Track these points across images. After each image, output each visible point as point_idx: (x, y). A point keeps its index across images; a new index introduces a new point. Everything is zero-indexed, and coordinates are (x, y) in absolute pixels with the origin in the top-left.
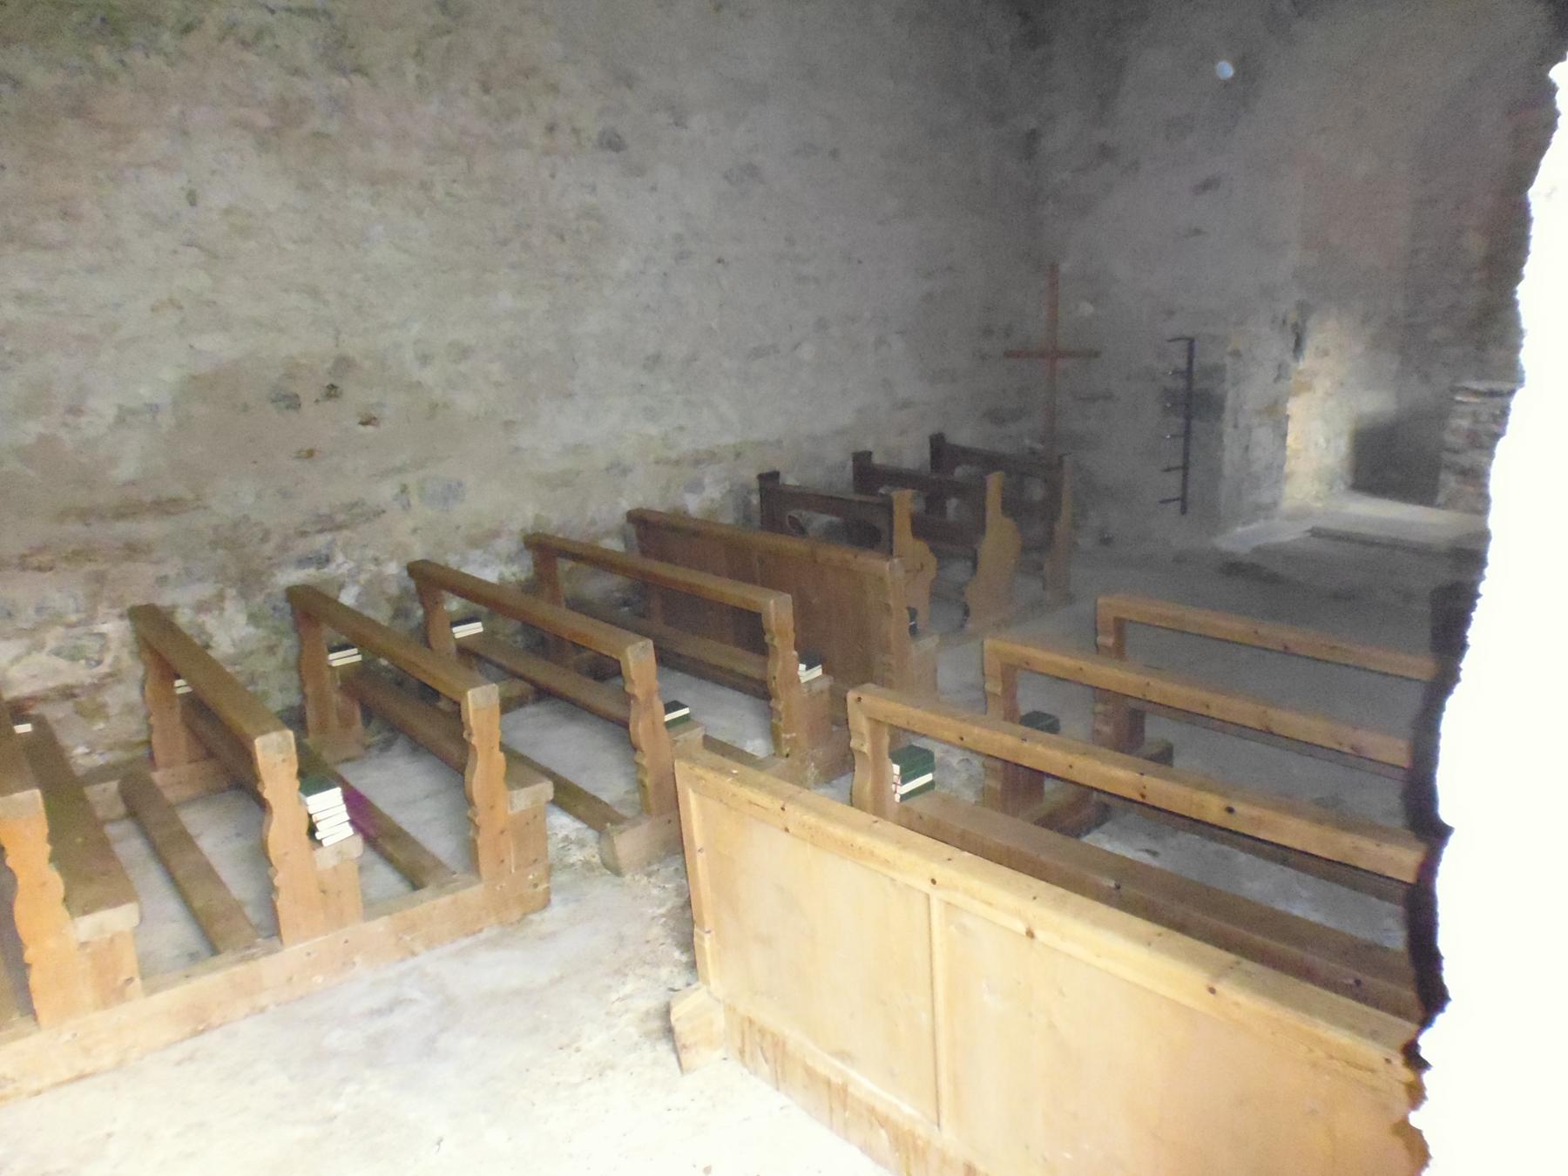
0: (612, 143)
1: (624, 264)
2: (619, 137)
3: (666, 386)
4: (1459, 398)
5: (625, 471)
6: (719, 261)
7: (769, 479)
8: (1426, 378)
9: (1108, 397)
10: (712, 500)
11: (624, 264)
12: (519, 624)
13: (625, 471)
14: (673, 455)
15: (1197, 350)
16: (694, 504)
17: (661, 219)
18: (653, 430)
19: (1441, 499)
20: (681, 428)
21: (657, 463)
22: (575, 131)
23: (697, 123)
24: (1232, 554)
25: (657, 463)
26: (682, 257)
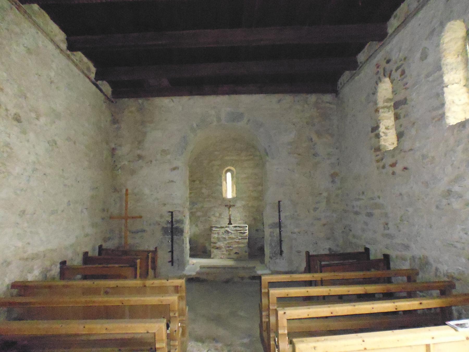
0: (17, 119)
1: (18, 170)
2: (20, 117)
3: (26, 225)
4: (214, 229)
5: (9, 264)
6: (45, 174)
7: (63, 263)
8: (197, 226)
9: (143, 231)
10: (36, 276)
11: (18, 170)
12: (438, 291)
13: (9, 264)
14: (25, 256)
15: (174, 216)
16: (30, 278)
17: (29, 153)
18: (20, 244)
19: (212, 256)
20: (29, 244)
21: (20, 259)
22: (7, 110)
23: (43, 120)
24: (190, 275)
25: (20, 259)
26: (35, 170)
